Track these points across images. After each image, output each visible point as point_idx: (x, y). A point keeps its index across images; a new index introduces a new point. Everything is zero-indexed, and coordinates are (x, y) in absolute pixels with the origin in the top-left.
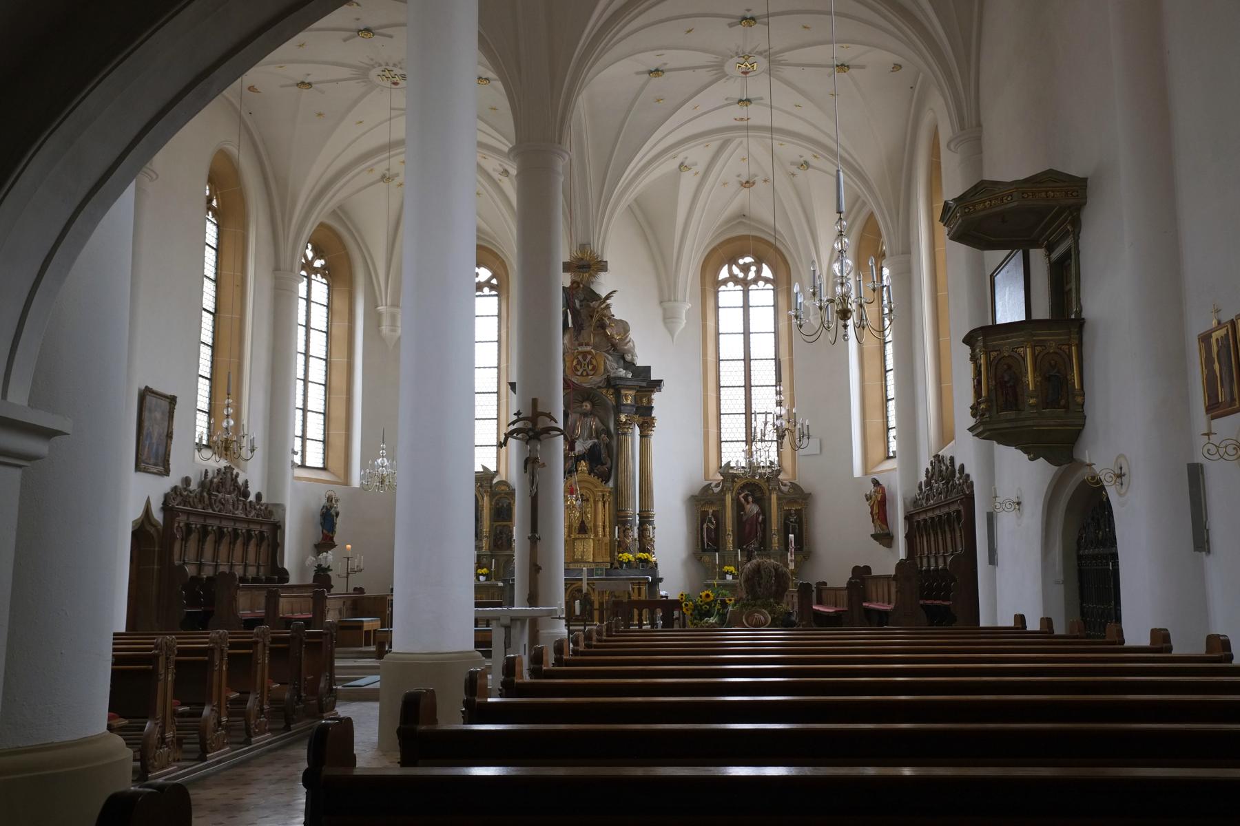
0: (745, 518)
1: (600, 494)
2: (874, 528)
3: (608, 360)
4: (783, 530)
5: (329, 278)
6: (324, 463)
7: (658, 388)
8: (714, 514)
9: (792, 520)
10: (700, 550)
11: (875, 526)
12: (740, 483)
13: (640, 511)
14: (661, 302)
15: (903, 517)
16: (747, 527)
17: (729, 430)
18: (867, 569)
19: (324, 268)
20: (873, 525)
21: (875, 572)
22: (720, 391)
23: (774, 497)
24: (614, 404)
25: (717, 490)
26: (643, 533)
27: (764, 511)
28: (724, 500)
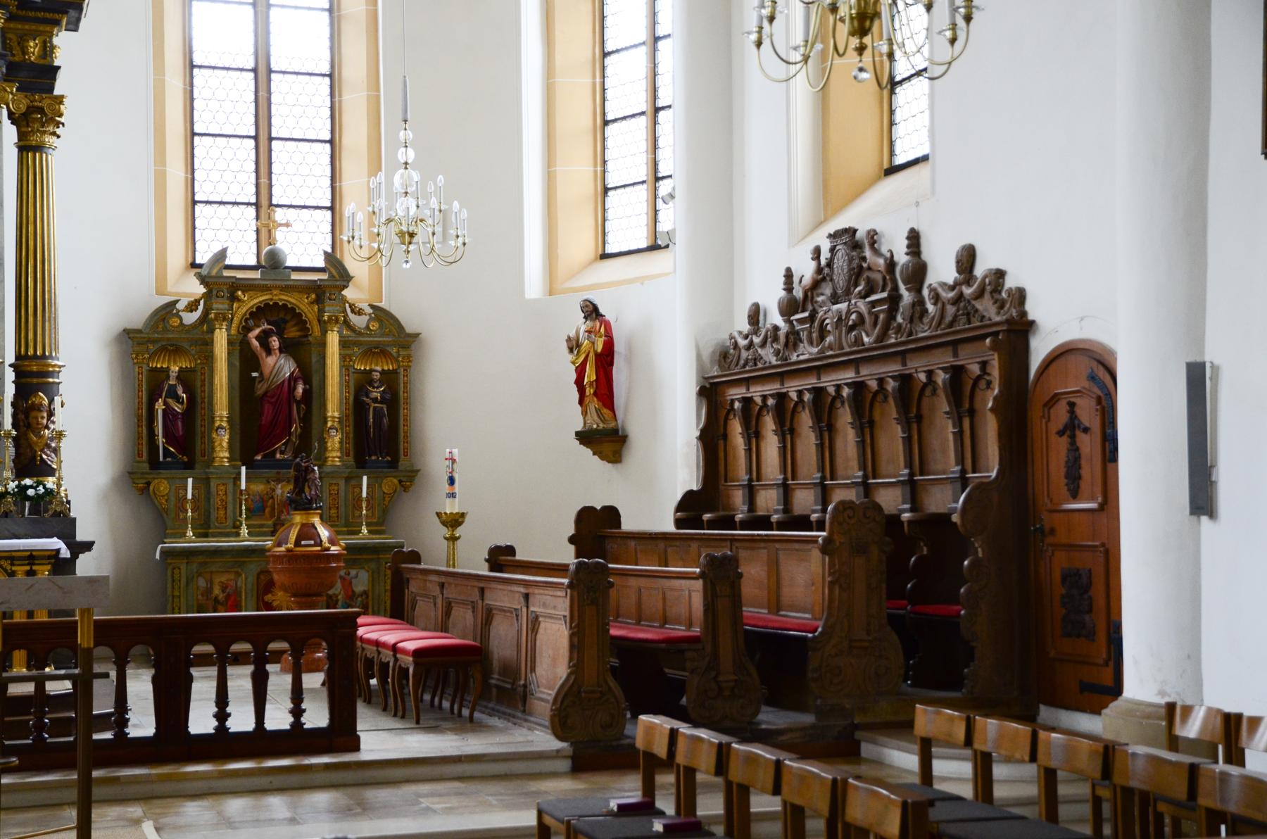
0: (261, 389)
2: (581, 418)
4: (351, 418)
7: (73, 13)
8: (183, 376)
9: (376, 394)
10: (146, 466)
11: (584, 413)
12: (249, 302)
13: (18, 357)
15: (694, 389)
16: (268, 409)
17: (215, 176)
18: (611, 514)
20: (579, 408)
21: (628, 525)
22: (192, 77)
23: (333, 339)
25: (190, 318)
26: (27, 417)
27: (310, 372)
28: (208, 344)
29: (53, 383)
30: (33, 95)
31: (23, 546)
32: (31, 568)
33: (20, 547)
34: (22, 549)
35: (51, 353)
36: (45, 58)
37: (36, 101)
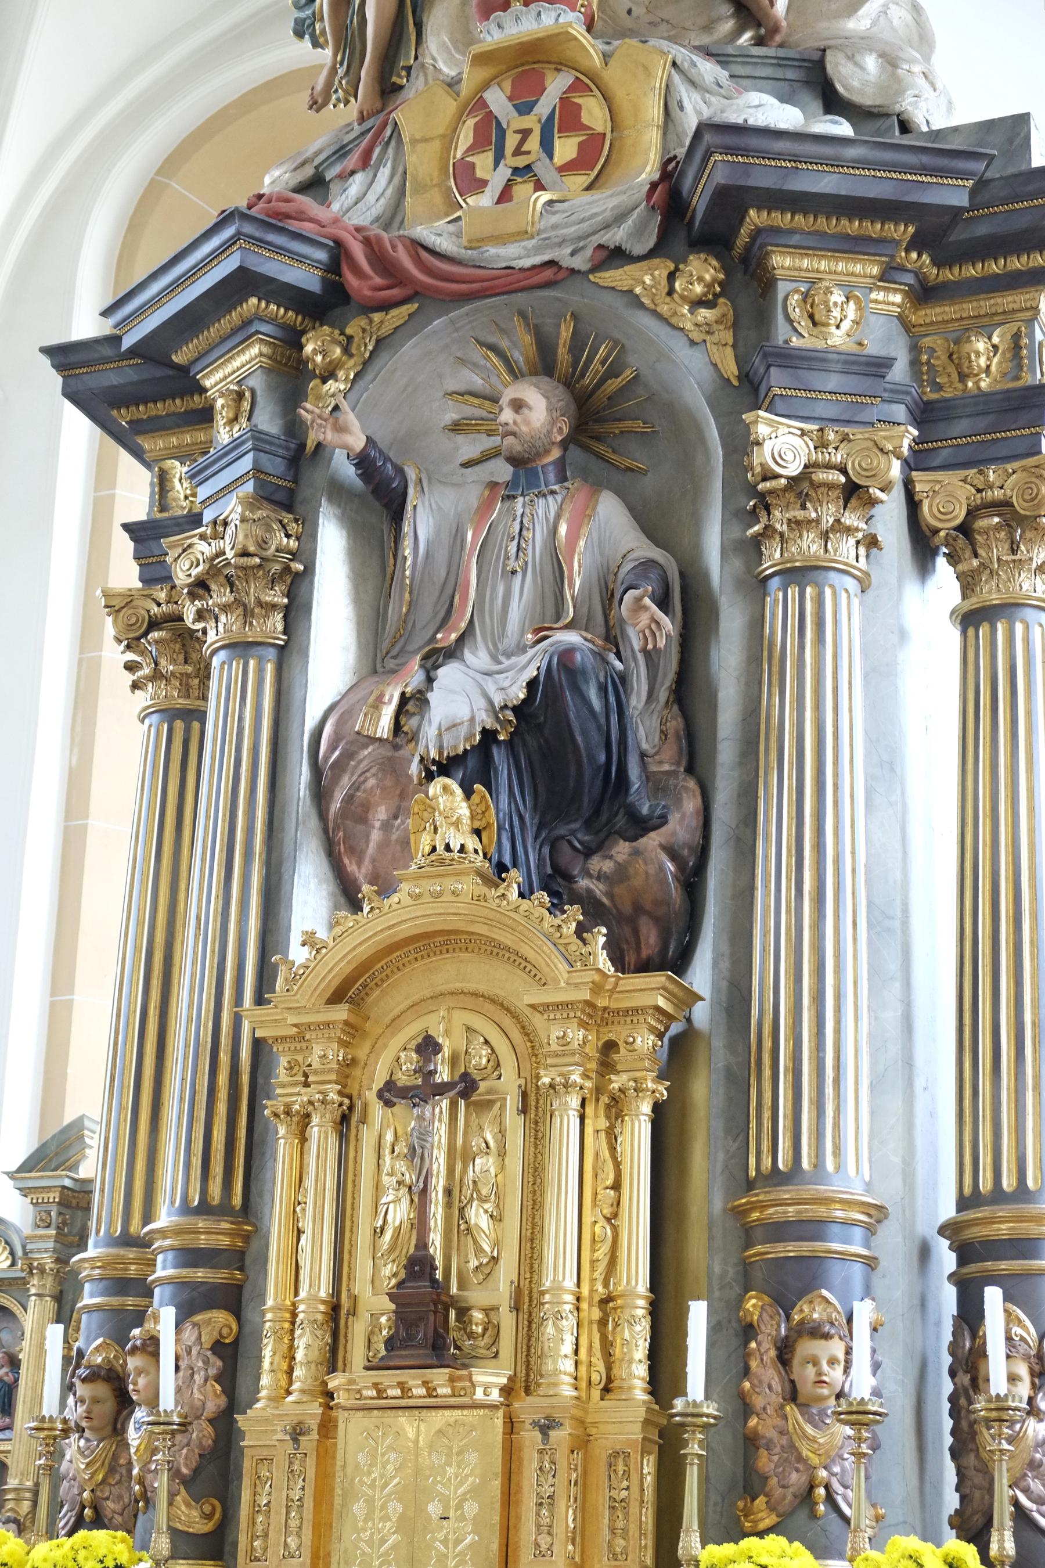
1: (576, 1035)
24: (731, 369)
30: (981, 472)
35: (818, 1163)
36: (1018, 378)
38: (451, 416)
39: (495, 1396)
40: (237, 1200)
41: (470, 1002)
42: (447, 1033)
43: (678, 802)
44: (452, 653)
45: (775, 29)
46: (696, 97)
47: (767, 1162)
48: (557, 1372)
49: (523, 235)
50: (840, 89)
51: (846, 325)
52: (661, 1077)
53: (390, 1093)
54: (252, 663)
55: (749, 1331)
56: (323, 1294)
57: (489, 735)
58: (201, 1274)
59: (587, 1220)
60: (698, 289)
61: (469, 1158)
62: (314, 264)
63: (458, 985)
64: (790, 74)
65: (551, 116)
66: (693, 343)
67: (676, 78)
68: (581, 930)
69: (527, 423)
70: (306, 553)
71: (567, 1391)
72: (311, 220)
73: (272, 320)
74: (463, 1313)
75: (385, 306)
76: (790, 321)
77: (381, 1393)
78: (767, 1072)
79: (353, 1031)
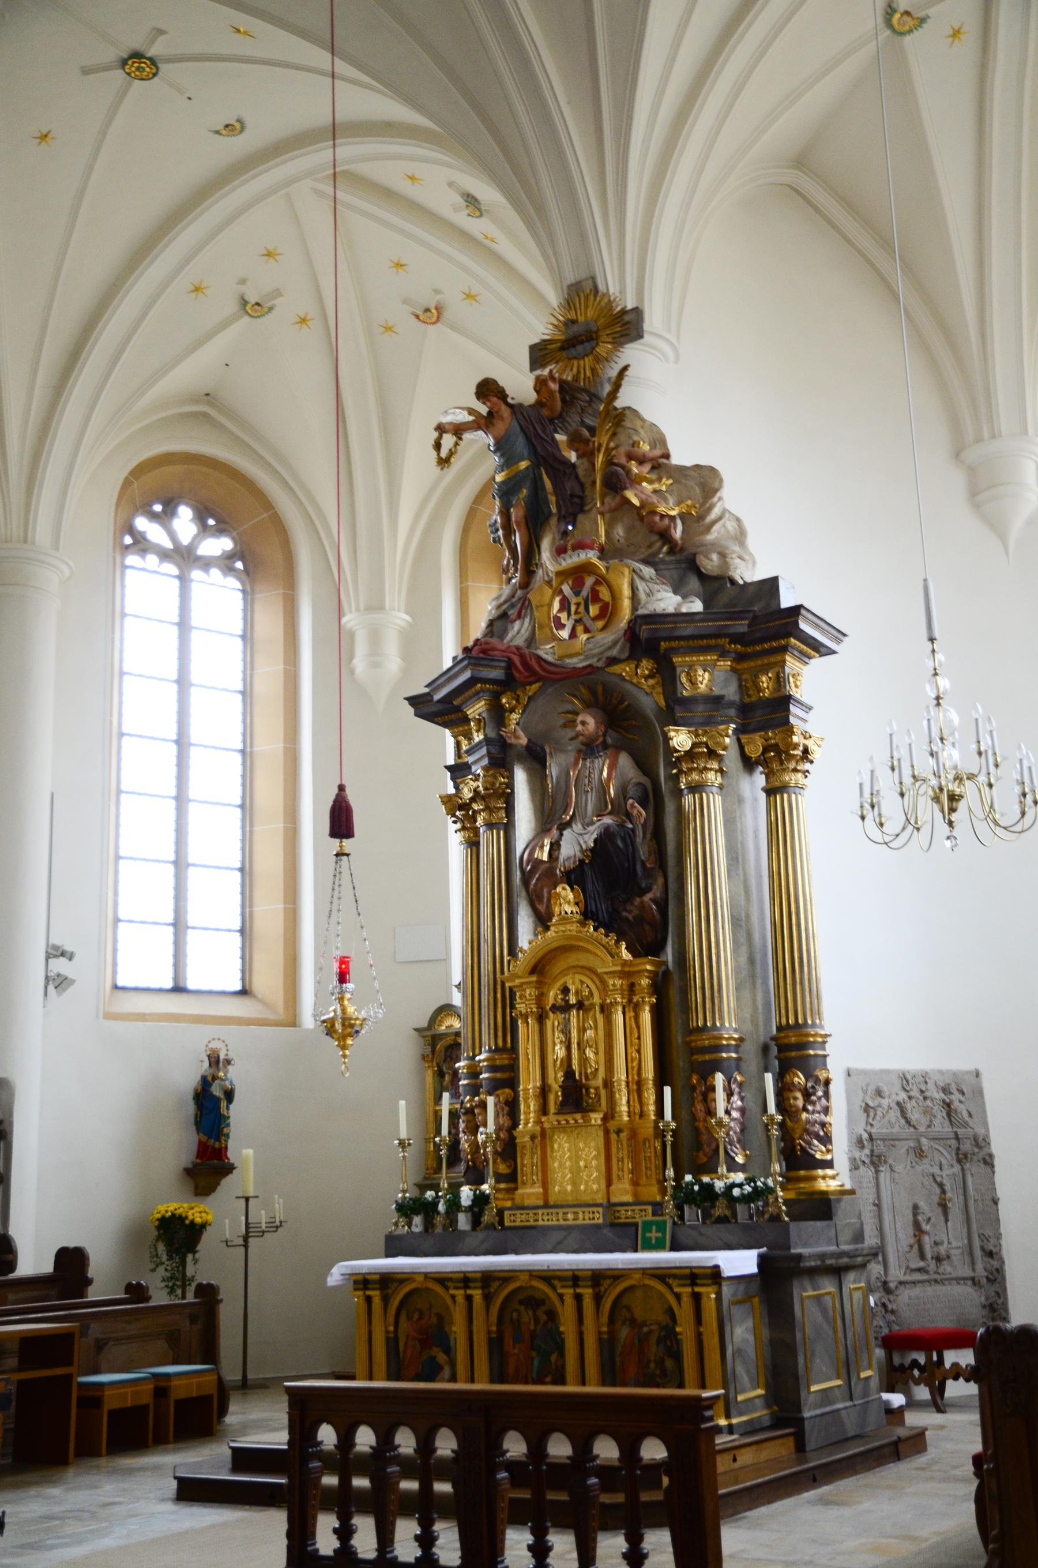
1: (618, 982)
3: (642, 578)
5: (244, 577)
6: (243, 979)
14: (957, 454)
19: (229, 557)
24: (662, 703)
29: (816, 1056)
31: (679, 1262)
32: (693, 1290)
33: (675, 1262)
34: (678, 1265)
35: (722, 1024)
36: (779, 691)
37: (771, 739)
38: (561, 722)
39: (599, 1122)
40: (509, 1045)
41: (579, 970)
42: (573, 983)
43: (656, 881)
44: (568, 824)
45: (676, 544)
46: (644, 584)
47: (695, 1024)
48: (621, 1112)
49: (577, 654)
50: (703, 570)
51: (705, 682)
52: (651, 995)
53: (555, 1008)
54: (495, 831)
55: (694, 1088)
56: (538, 1085)
57: (581, 861)
58: (498, 1075)
59: (629, 1051)
60: (647, 672)
61: (584, 1030)
62: (501, 668)
63: (576, 963)
64: (683, 566)
65: (587, 597)
66: (647, 693)
67: (635, 577)
68: (617, 942)
69: (588, 730)
70: (511, 785)
71: (626, 1118)
72: (498, 650)
73: (489, 690)
74: (587, 1090)
75: (530, 684)
76: (682, 684)
77: (559, 1122)
78: (693, 989)
79: (540, 985)
